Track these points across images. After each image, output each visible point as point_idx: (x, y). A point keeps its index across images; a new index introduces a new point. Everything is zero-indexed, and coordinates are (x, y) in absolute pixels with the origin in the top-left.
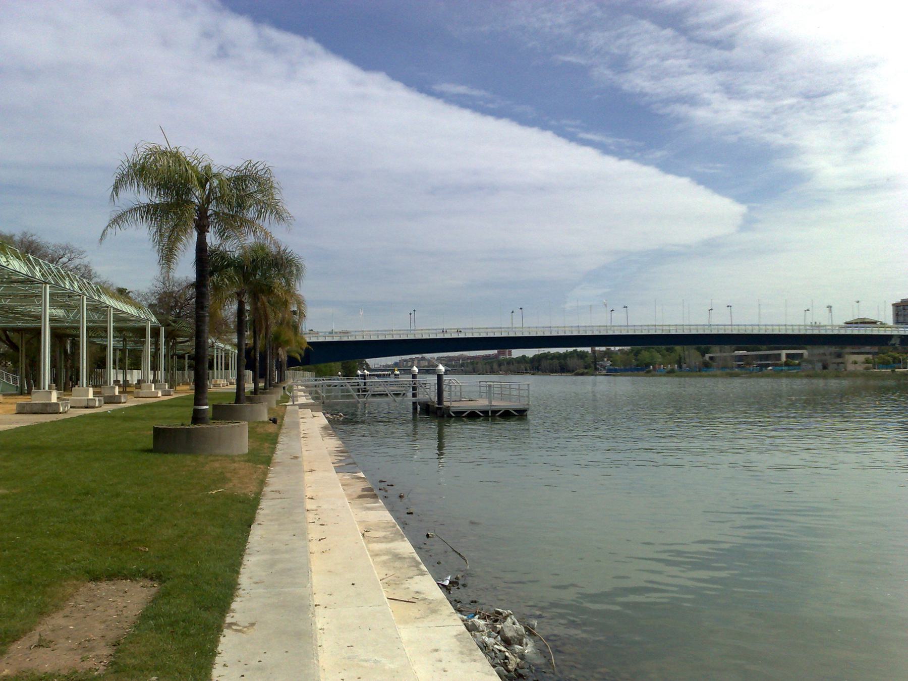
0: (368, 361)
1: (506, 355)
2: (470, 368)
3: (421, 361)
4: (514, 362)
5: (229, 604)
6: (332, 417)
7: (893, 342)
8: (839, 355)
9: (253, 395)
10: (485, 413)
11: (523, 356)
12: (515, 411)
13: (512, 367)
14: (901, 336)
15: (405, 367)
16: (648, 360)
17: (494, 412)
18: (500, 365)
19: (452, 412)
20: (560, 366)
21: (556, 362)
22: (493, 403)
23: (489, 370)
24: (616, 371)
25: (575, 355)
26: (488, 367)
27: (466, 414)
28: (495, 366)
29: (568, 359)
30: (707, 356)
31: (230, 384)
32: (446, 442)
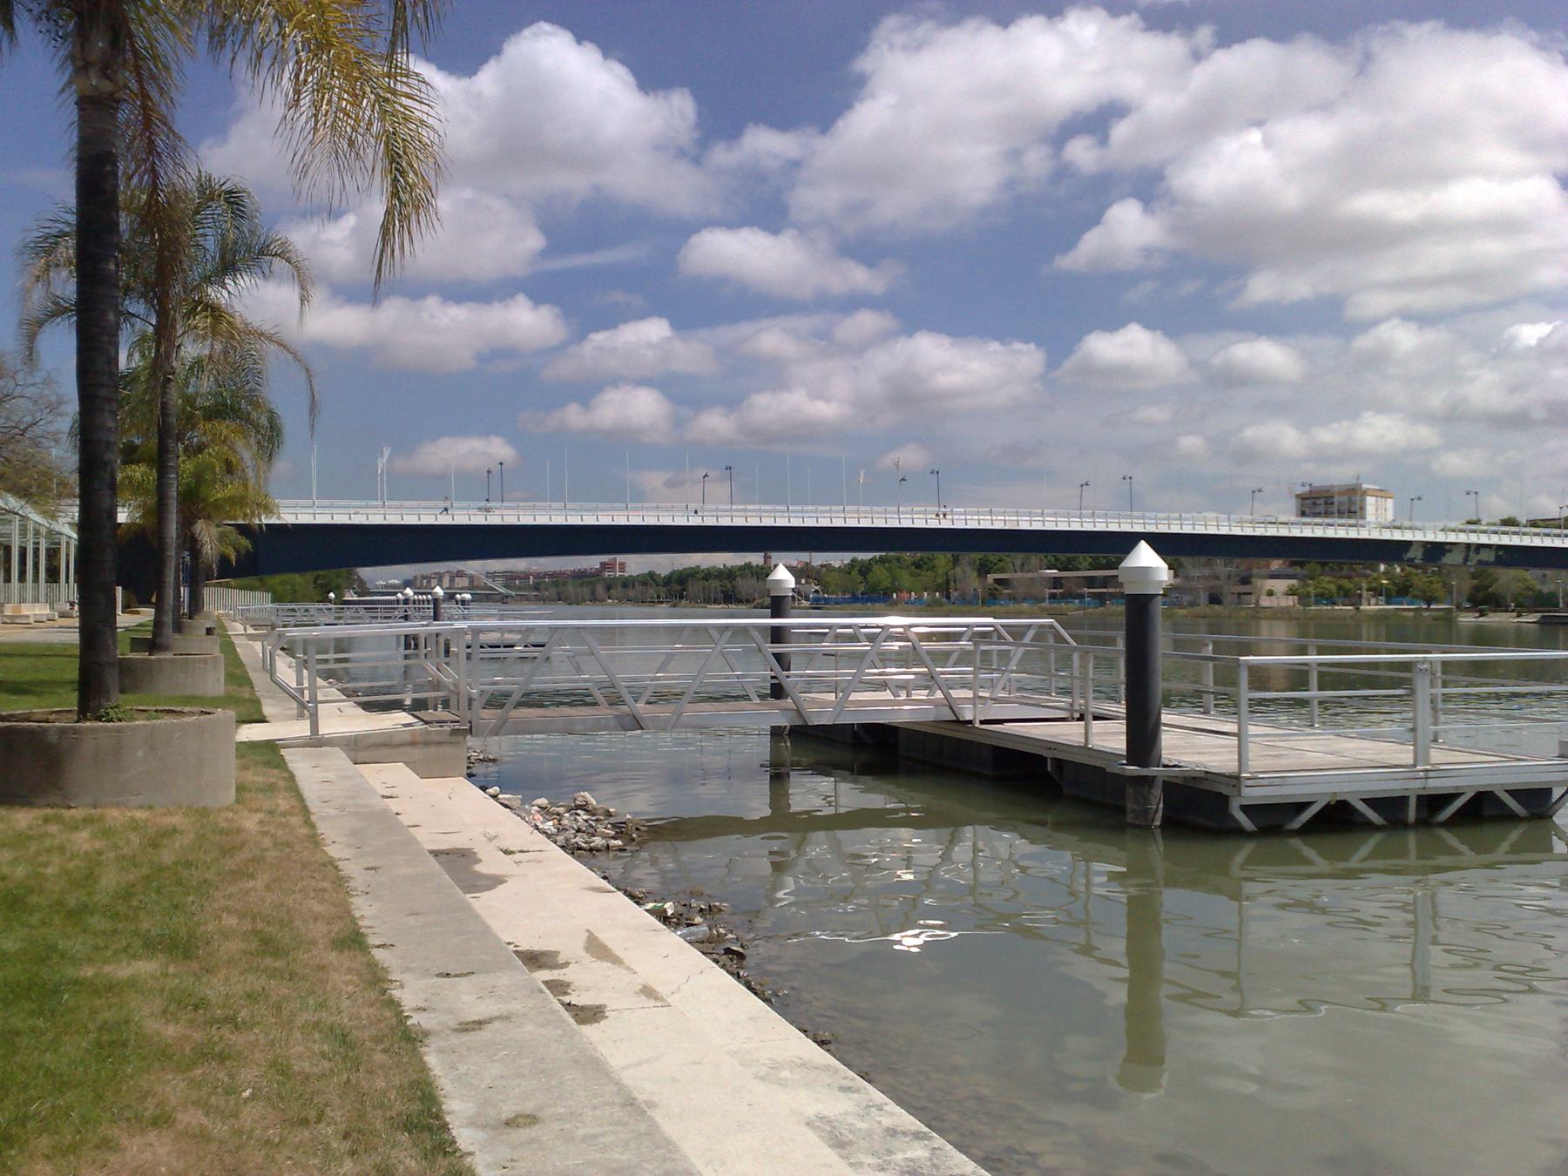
0: (365, 572)
1: (615, 571)
2: (553, 592)
3: (457, 579)
4: (636, 584)
5: (79, 164)
6: (899, 1157)
7: (1410, 555)
8: (1245, 581)
9: (145, 655)
10: (1390, 807)
11: (650, 572)
12: (1515, 793)
13: (631, 593)
14: (1425, 544)
15: (426, 588)
16: (886, 583)
17: (1433, 803)
18: (608, 588)
19: (1245, 808)
20: (722, 591)
21: (715, 584)
22: (1437, 756)
23: (587, 597)
24: (827, 601)
25: (748, 571)
26: (586, 590)
27: (1306, 816)
28: (600, 590)
29: (738, 579)
30: (991, 577)
31: (60, 617)
32: (634, 721)
